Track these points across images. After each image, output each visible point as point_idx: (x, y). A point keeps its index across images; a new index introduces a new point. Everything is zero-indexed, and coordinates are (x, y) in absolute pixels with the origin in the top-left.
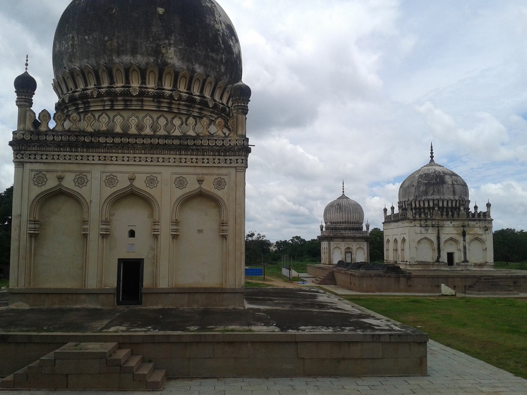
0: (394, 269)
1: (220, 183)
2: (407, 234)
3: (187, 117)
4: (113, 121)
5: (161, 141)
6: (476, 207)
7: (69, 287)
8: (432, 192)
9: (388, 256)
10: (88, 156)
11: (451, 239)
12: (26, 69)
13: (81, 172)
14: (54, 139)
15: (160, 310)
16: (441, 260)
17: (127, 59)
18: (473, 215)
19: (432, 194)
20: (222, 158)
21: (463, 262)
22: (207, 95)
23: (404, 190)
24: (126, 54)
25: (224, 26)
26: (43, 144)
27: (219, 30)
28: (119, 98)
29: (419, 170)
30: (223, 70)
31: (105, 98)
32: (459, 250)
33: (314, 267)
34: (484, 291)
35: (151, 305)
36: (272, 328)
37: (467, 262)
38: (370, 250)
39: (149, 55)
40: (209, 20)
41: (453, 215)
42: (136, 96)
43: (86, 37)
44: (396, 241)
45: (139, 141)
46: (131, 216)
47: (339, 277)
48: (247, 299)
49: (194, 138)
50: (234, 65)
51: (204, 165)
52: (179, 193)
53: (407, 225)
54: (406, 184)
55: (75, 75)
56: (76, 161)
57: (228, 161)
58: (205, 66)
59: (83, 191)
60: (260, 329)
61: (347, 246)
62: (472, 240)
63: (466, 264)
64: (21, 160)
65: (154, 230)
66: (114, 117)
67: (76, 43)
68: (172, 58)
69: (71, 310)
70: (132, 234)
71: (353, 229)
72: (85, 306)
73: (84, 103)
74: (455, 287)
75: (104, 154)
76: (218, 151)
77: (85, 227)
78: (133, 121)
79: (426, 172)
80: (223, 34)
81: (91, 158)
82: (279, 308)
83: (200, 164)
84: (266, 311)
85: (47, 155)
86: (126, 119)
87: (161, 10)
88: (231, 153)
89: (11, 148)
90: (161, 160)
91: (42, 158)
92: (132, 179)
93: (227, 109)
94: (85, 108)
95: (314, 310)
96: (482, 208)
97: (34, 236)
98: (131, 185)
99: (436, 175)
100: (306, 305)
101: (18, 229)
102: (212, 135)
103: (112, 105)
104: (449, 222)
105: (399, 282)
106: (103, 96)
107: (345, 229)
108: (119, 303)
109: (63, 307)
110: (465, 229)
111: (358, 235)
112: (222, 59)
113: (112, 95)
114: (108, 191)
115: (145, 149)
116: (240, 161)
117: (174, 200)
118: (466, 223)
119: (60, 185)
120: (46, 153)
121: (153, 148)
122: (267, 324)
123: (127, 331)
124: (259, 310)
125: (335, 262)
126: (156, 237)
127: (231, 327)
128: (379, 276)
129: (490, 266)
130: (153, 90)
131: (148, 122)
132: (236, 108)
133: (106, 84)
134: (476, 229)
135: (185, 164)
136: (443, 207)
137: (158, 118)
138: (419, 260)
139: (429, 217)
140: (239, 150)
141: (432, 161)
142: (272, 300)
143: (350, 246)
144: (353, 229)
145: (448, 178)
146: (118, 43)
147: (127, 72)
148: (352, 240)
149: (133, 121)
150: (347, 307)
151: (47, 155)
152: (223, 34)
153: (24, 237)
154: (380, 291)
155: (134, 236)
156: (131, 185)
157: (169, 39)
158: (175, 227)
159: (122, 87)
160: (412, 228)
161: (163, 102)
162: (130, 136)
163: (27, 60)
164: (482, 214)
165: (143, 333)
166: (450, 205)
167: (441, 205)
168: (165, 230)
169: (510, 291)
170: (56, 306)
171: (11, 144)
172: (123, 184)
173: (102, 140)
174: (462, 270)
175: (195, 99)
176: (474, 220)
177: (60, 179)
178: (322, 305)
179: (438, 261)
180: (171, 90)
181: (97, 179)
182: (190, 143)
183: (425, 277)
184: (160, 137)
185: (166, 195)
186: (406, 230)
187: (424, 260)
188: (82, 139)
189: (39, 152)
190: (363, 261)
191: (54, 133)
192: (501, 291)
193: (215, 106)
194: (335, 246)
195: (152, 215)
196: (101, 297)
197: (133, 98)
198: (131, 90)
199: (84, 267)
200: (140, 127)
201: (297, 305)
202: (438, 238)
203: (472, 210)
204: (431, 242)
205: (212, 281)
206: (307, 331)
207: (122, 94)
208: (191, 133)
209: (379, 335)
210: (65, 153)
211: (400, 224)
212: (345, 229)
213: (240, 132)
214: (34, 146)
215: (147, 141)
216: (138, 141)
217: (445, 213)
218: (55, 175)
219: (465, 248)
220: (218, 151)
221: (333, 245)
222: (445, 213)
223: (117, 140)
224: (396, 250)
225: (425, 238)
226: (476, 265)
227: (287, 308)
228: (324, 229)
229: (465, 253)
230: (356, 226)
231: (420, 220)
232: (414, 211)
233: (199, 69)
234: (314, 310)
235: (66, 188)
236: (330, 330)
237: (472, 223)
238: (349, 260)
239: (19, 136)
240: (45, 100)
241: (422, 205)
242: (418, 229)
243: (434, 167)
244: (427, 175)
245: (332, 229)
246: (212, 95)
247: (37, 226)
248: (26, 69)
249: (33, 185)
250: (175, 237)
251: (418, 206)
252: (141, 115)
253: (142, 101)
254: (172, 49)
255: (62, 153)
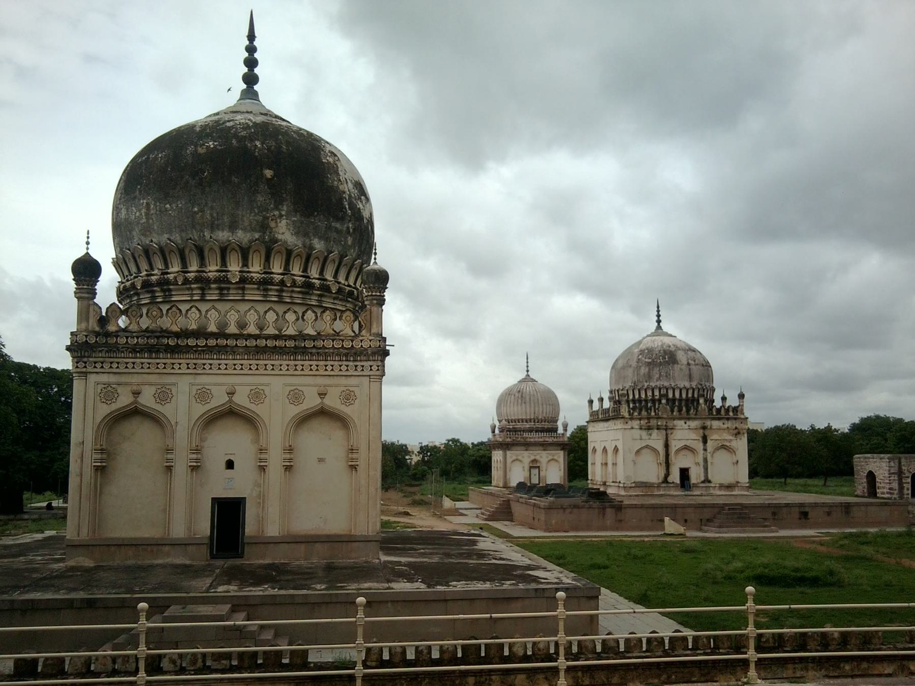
0: (599, 496)
1: (348, 397)
2: (621, 440)
3: (304, 309)
4: (206, 317)
5: (270, 343)
6: (724, 399)
7: (147, 536)
8: (657, 376)
9: (594, 474)
10: (173, 364)
11: (686, 448)
12: (88, 249)
13: (164, 385)
14: (127, 342)
15: (269, 565)
16: (670, 479)
17: (223, 235)
18: (719, 411)
19: (659, 379)
20: (351, 364)
21: (703, 482)
22: (329, 276)
23: (617, 370)
24: (223, 230)
25: (350, 185)
26: (113, 349)
27: (344, 192)
28: (213, 286)
29: (640, 342)
30: (350, 243)
31: (193, 286)
32: (697, 464)
33: (480, 492)
34: (727, 527)
35: (254, 559)
36: (417, 585)
37: (710, 482)
38: (569, 463)
39: (253, 230)
40: (332, 181)
41: (688, 411)
42: (236, 283)
43: (168, 206)
44: (605, 450)
45: (241, 343)
46: (229, 441)
47: (517, 509)
48: (382, 549)
49: (313, 338)
50: (363, 235)
51: (326, 373)
52: (294, 411)
53: (620, 426)
54: (620, 364)
55: (151, 254)
56: (158, 371)
57: (359, 368)
58: (327, 240)
59: (166, 410)
60: (402, 586)
61: (533, 458)
62: (718, 449)
63: (708, 484)
64: (84, 370)
65: (261, 460)
66: (207, 311)
67: (152, 212)
68: (283, 233)
69: (152, 566)
70: (233, 465)
71: (543, 430)
72: (169, 560)
73: (163, 291)
74: (686, 521)
75: (195, 361)
76: (346, 355)
77: (169, 456)
78: (233, 317)
79: (650, 345)
80: (350, 196)
81: (176, 366)
82: (425, 560)
83: (322, 372)
84: (409, 565)
85: (118, 363)
86: (223, 313)
87: (268, 173)
88: (363, 358)
89: (68, 353)
90: (270, 367)
91: (111, 367)
92: (231, 393)
93: (355, 292)
94: (165, 297)
95: (471, 562)
96: (732, 401)
97: (101, 470)
98: (230, 401)
99: (665, 351)
100: (461, 555)
101: (79, 461)
102: (338, 334)
103: (203, 295)
104: (682, 422)
105: (604, 514)
106: (190, 283)
107: (530, 430)
108: (213, 557)
109: (140, 563)
110: (707, 432)
111: (550, 440)
112: (348, 228)
113: (203, 282)
114: (200, 410)
115: (248, 353)
116: (375, 368)
117: (287, 419)
118: (708, 423)
119: (136, 402)
120: (116, 360)
121: (260, 351)
122: (411, 580)
123: (240, 590)
124: (399, 563)
125: (514, 483)
126: (262, 469)
127: (366, 585)
128: (576, 506)
129: (743, 488)
130: (258, 275)
131: (252, 317)
132: (369, 298)
133: (194, 267)
134: (720, 431)
135: (302, 373)
136: (674, 400)
137: (266, 312)
138: (638, 480)
139: (653, 414)
140: (374, 354)
141: (659, 327)
142: (416, 550)
143: (538, 457)
144: (543, 430)
145: (681, 357)
146: (211, 215)
147: (224, 251)
148: (541, 448)
149: (233, 317)
150: (517, 557)
151: (118, 363)
152: (350, 196)
153: (88, 472)
154: (576, 529)
155: (232, 468)
156: (230, 401)
157: (279, 210)
158: (288, 456)
159: (218, 271)
160: (628, 432)
161: (271, 290)
162: (227, 336)
163: (88, 238)
164: (731, 409)
165: (261, 593)
166: (684, 396)
167: (671, 396)
168: (275, 459)
169: (766, 526)
170: (130, 562)
171: (68, 348)
172: (219, 399)
173: (191, 342)
174: (701, 495)
175: (314, 284)
176: (719, 419)
177: (137, 394)
178: (481, 555)
179: (665, 481)
180: (281, 274)
181: (184, 392)
182: (309, 344)
183: (642, 506)
184: (267, 337)
185: (277, 414)
186: (619, 435)
187: (644, 479)
188: (165, 341)
189: (107, 360)
190: (558, 482)
191: (128, 334)
192: (752, 527)
193: (340, 290)
194: (514, 458)
195: (257, 440)
196: (190, 548)
197: (232, 286)
198: (229, 275)
199: (167, 510)
200: (242, 325)
201: (448, 555)
202: (667, 446)
203: (718, 403)
204: (654, 450)
205: (337, 525)
206: (459, 586)
207: (217, 280)
208: (310, 331)
209: (543, 589)
210: (143, 360)
211: (610, 424)
212: (530, 430)
213: (374, 330)
214: (101, 351)
215: (252, 343)
216: (239, 343)
217: (676, 408)
218: (129, 388)
219: (705, 460)
220: (346, 355)
221: (511, 457)
222: (676, 408)
223: (212, 342)
224: (606, 464)
225: (647, 447)
226: (721, 486)
227: (436, 559)
228: (497, 431)
229: (706, 469)
230: (546, 425)
231: (640, 419)
232: (631, 405)
233: (319, 245)
234: (471, 562)
235: (143, 405)
236: (487, 586)
237: (716, 424)
238: (535, 481)
239: (81, 338)
240: (109, 283)
241: (643, 396)
242: (637, 433)
243: (662, 338)
244: (650, 350)
245: (509, 430)
246: (336, 276)
247: (104, 456)
248: (88, 249)
249: (99, 402)
250: (288, 468)
251: (637, 397)
252: (243, 307)
253: (243, 289)
254: (284, 222)
255: (138, 361)
